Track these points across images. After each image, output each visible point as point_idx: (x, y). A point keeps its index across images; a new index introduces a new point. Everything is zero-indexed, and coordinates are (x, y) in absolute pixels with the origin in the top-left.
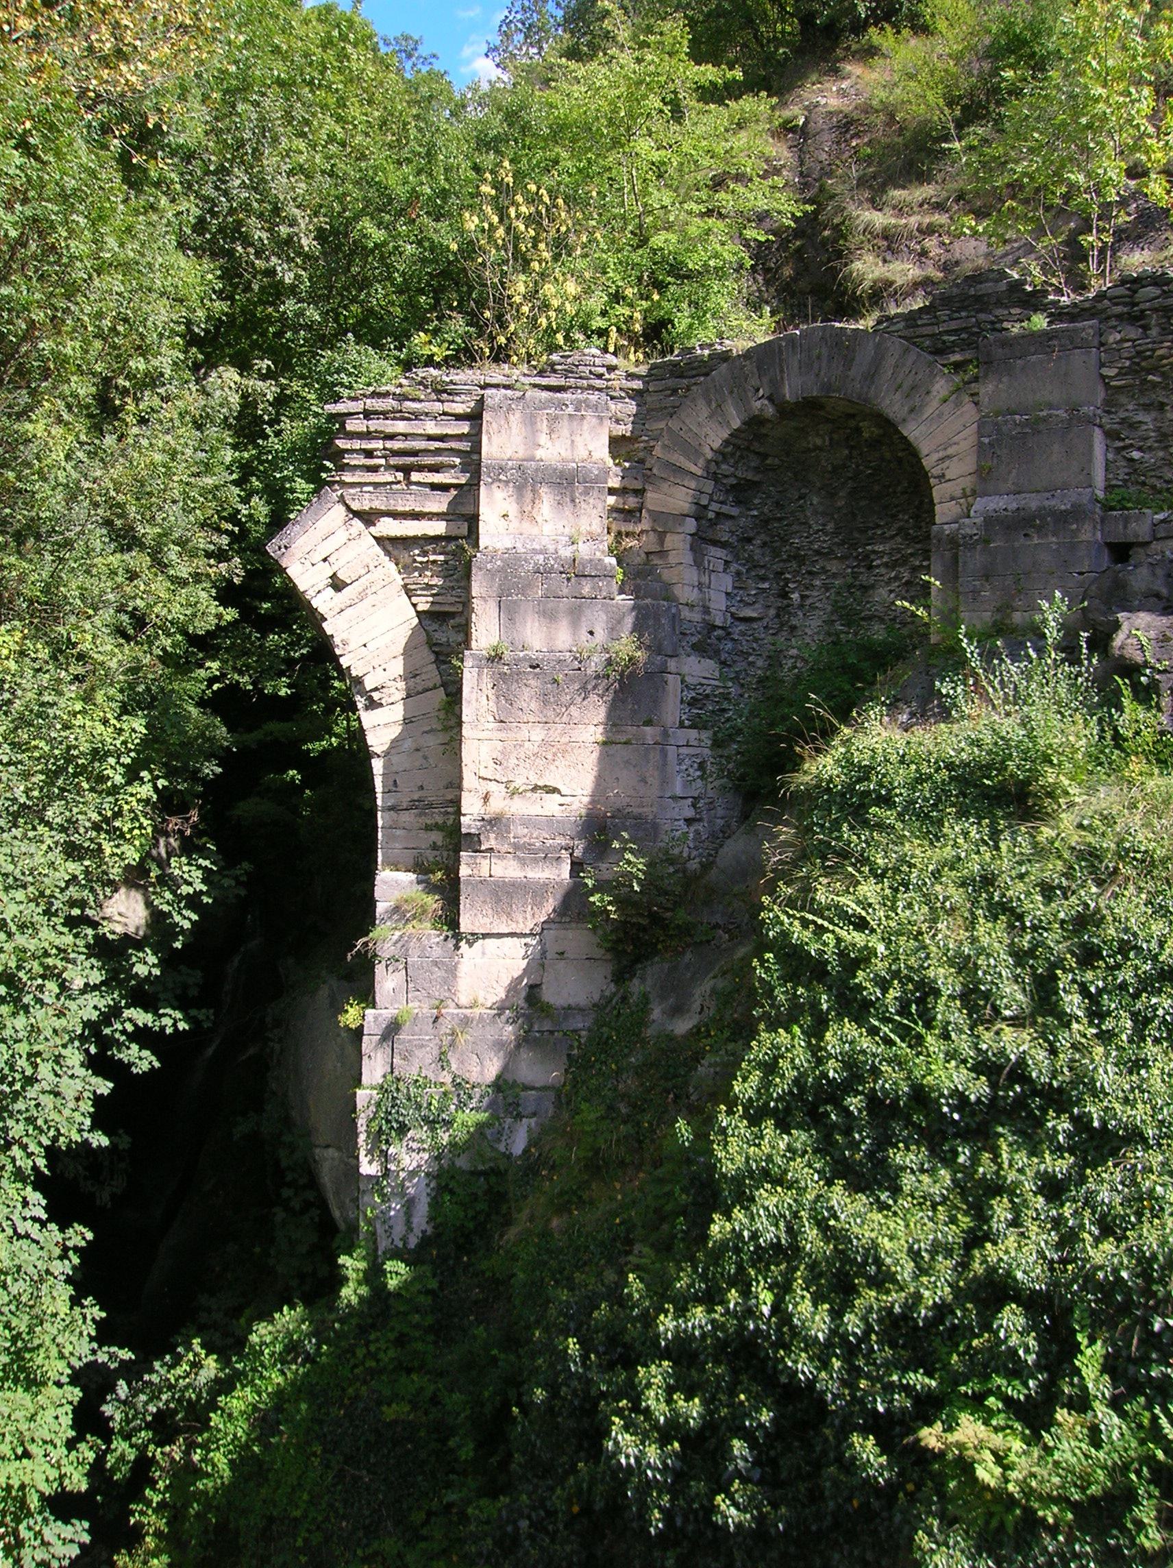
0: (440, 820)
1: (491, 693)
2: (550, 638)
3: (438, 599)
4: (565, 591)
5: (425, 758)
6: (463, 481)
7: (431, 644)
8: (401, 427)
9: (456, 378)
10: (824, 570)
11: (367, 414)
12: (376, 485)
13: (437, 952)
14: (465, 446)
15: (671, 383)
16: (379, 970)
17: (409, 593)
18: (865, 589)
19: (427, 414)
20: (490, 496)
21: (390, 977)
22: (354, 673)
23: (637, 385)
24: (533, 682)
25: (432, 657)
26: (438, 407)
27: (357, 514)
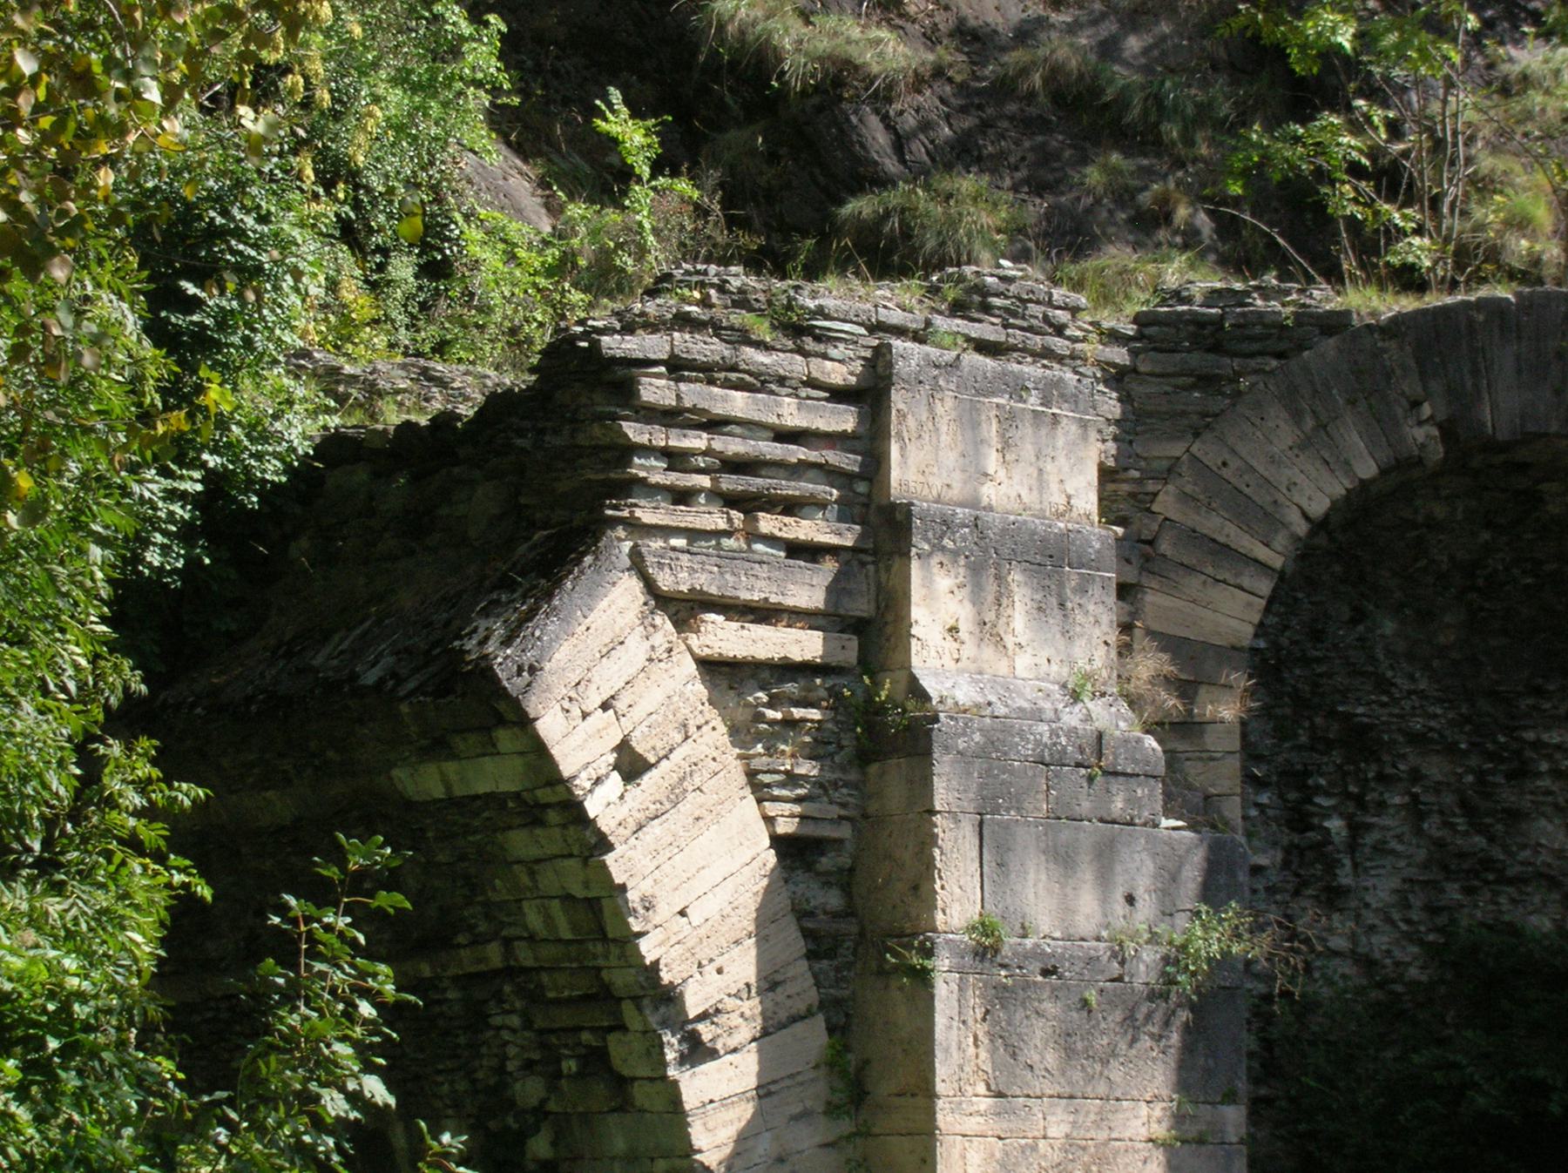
1: (981, 1030)
2: (1066, 910)
3: (811, 809)
4: (1086, 806)
6: (849, 542)
7: (802, 914)
8: (738, 403)
9: (830, 303)
10: (1416, 776)
11: (677, 367)
12: (693, 534)
14: (847, 461)
15: (1196, 360)
17: (761, 793)
18: (1514, 816)
19: (782, 381)
20: (928, 583)
23: (1120, 355)
24: (1049, 1007)
25: (800, 946)
26: (796, 366)
27: (660, 600)
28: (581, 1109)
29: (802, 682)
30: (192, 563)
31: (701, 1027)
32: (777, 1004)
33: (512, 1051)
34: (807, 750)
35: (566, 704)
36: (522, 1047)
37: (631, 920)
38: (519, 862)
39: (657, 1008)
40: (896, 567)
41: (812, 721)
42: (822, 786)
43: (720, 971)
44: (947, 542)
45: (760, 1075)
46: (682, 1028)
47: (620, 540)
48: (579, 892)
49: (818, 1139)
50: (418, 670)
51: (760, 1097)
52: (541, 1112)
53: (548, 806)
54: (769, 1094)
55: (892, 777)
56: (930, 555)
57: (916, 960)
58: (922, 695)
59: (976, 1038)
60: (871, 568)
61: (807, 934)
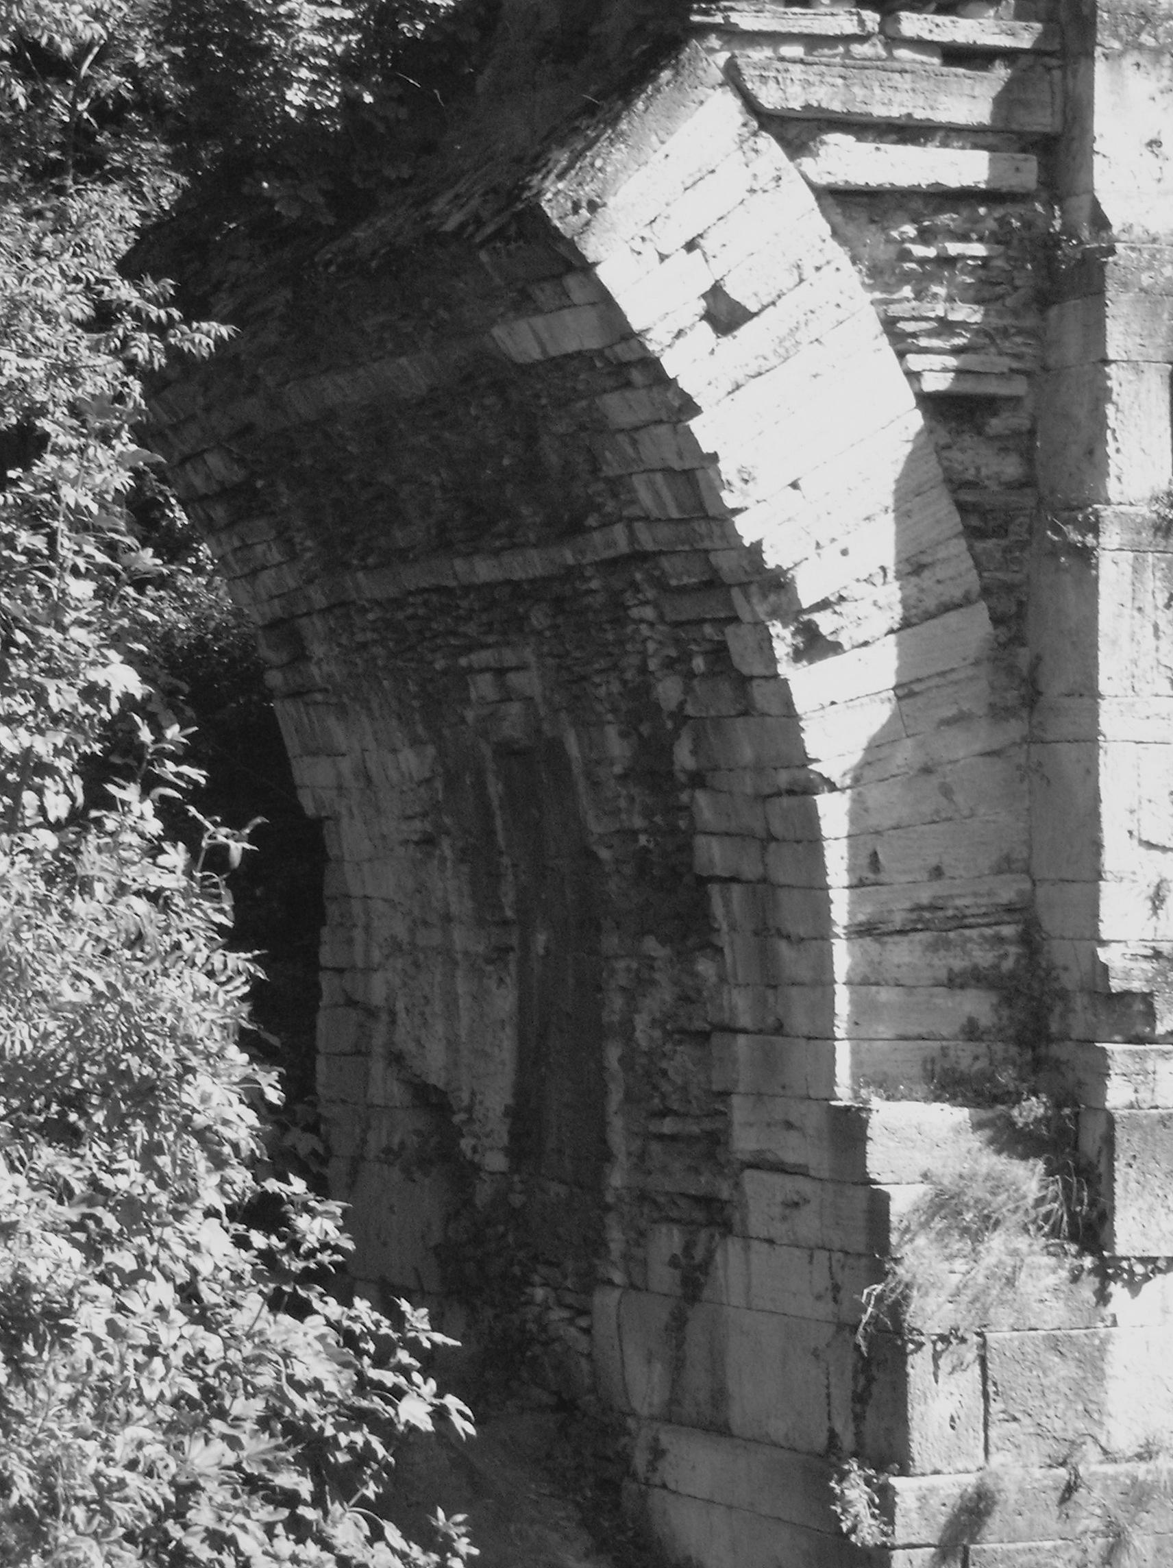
0: (983, 957)
3: (971, 361)
5: (946, 791)
6: (1025, 41)
7: (956, 484)
12: (813, 41)
13: (1054, 1314)
16: (918, 1366)
17: (902, 344)
21: (947, 1383)
22: (771, 560)
25: (955, 521)
28: (713, 713)
29: (966, 213)
30: (350, 103)
31: (817, 617)
32: (922, 590)
33: (651, 646)
34: (971, 293)
35: (638, 244)
36: (660, 643)
37: (724, 494)
38: (622, 430)
39: (765, 597)
40: (1082, 70)
41: (974, 258)
42: (987, 334)
43: (844, 552)
44: (1145, 39)
45: (899, 671)
46: (796, 619)
47: (711, 51)
48: (677, 465)
49: (978, 747)
50: (499, 212)
51: (899, 698)
52: (680, 717)
53: (629, 364)
54: (912, 694)
55: (1071, 311)
56: (1121, 54)
57: (1075, 537)
58: (1100, 222)
59: (1156, 628)
60: (1057, 74)
61: (962, 508)
